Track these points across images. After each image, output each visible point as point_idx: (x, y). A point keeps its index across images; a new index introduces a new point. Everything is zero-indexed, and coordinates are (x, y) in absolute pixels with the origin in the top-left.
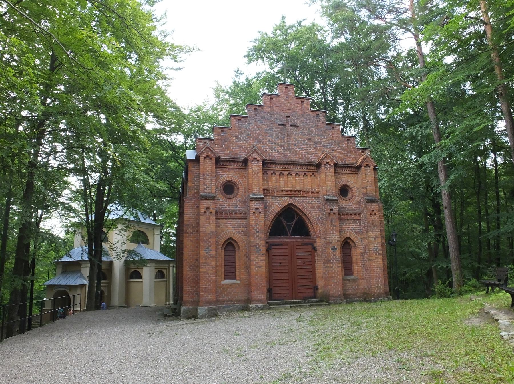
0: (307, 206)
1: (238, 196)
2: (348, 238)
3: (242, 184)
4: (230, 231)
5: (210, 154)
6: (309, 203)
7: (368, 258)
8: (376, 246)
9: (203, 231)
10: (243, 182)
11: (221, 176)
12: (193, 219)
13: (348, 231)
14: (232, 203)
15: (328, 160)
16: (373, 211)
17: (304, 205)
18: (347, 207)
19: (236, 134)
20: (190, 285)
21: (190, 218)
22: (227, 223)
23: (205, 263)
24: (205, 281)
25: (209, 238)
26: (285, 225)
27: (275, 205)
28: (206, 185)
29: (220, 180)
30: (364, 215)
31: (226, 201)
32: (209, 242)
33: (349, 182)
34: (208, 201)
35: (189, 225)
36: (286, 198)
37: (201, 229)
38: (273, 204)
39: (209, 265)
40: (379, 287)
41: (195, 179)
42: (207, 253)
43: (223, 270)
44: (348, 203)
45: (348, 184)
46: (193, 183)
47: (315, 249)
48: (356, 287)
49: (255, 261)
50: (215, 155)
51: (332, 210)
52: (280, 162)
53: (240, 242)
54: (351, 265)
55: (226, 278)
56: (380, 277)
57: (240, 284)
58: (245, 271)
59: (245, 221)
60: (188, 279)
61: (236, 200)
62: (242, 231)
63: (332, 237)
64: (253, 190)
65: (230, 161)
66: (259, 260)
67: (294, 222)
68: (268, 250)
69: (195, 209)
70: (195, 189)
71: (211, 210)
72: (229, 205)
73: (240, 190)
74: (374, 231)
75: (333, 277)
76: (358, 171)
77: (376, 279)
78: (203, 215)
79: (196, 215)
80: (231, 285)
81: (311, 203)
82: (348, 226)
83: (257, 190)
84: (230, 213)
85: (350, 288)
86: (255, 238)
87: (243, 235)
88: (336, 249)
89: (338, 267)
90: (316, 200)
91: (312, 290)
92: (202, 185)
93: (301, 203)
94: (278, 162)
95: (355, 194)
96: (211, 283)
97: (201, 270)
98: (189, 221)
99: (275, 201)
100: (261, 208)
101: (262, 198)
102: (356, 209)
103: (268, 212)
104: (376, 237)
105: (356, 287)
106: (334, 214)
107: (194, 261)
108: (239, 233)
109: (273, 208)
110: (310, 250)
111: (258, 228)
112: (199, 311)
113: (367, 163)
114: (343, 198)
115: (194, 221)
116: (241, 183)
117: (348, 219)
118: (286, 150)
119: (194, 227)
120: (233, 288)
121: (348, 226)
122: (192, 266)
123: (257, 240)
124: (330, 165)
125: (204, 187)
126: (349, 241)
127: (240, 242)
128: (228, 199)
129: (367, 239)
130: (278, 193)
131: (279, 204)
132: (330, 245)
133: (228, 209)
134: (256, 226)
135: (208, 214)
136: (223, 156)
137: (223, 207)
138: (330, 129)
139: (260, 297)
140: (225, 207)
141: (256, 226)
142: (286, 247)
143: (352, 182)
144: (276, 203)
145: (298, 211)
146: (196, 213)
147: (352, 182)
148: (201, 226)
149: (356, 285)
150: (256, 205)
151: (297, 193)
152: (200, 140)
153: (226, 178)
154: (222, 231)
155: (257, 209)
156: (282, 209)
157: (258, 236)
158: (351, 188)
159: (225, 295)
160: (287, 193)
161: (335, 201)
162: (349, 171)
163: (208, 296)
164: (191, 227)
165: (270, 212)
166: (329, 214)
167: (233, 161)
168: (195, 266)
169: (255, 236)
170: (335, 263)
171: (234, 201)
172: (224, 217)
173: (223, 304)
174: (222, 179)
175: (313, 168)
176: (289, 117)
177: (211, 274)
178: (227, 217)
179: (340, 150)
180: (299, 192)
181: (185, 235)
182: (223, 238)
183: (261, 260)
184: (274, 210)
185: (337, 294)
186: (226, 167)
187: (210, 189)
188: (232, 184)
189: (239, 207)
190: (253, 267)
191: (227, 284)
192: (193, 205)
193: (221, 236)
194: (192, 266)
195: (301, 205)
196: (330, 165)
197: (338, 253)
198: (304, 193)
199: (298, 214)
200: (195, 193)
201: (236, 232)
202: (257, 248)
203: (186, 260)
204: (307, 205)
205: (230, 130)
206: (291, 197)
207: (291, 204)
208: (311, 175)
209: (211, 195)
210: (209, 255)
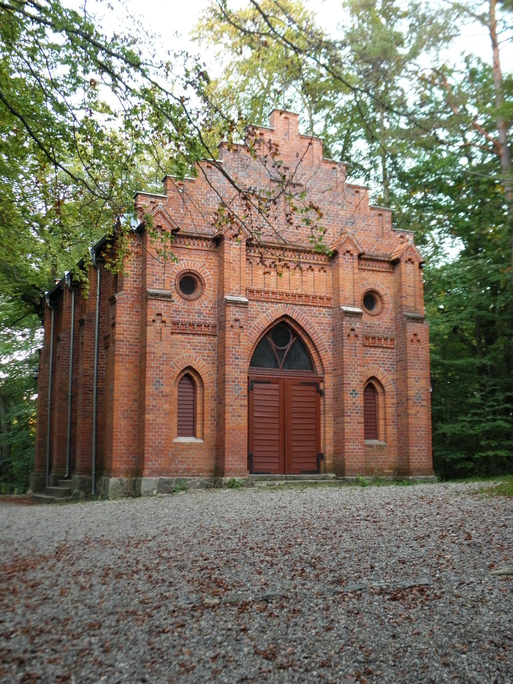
0: (312, 320)
1: (203, 298)
2: (373, 378)
3: (210, 277)
4: (190, 356)
5: (162, 223)
6: (315, 317)
7: (404, 412)
8: (418, 393)
9: (150, 353)
10: (211, 275)
11: (177, 262)
12: (130, 331)
13: (373, 367)
14: (193, 309)
15: (350, 248)
16: (415, 335)
17: (306, 319)
18: (373, 327)
19: (202, 192)
20: (123, 442)
21: (124, 330)
22: (184, 342)
23: (153, 406)
24: (153, 436)
25: (160, 364)
26: (274, 350)
27: (262, 316)
28: (155, 276)
29: (176, 269)
30: (401, 342)
31: (184, 305)
32: (160, 371)
33: (378, 285)
34: (160, 303)
35: (122, 341)
36: (280, 305)
37: (148, 349)
38: (258, 315)
39: (158, 410)
40: (421, 459)
41: (133, 264)
42: (156, 389)
43: (176, 420)
44: (375, 321)
45: (377, 289)
46: (131, 271)
47: (321, 393)
48: (382, 458)
49: (232, 406)
50: (172, 226)
51: (353, 330)
52: (272, 245)
53: (205, 374)
54: (376, 422)
55: (180, 435)
56: (422, 443)
57: (203, 444)
58: (211, 424)
59: (213, 340)
60: (120, 432)
61: (201, 304)
62: (208, 356)
63: (351, 375)
64: (230, 289)
65: (192, 238)
66: (237, 406)
67: (288, 346)
68: (250, 389)
69: (134, 315)
70: (135, 281)
71: (164, 318)
72: (188, 312)
73: (207, 287)
74: (417, 369)
75: (351, 439)
76: (393, 269)
77: (416, 446)
78: (152, 326)
79: (135, 325)
80: (190, 446)
81: (318, 317)
82: (374, 357)
83: (236, 290)
84: (190, 325)
85: (372, 459)
86: (233, 368)
87: (209, 363)
88: (356, 394)
89: (359, 423)
90: (326, 311)
91: (314, 460)
92: (150, 274)
93: (302, 315)
94: (270, 245)
95: (386, 306)
96: (162, 439)
97: (147, 416)
98: (123, 334)
99: (261, 309)
100: (243, 319)
101: (246, 304)
102: (388, 331)
103: (250, 327)
104: (419, 378)
105: (382, 458)
106: (356, 336)
107: (131, 403)
108: (204, 360)
109: (258, 321)
110: (313, 394)
111: (238, 352)
112: (143, 483)
113: (410, 257)
114: (367, 311)
115: (132, 335)
116: (208, 276)
117: (375, 347)
118: (281, 225)
119: (132, 345)
120: (192, 450)
121: (374, 357)
122: (127, 411)
123: (236, 372)
124: (351, 255)
125: (153, 279)
126: (373, 382)
127: (205, 374)
128: (186, 302)
129: (404, 382)
130: (274, 297)
131: (267, 315)
132: (347, 387)
133: (187, 319)
134: (235, 348)
135: (158, 324)
136: (184, 230)
137: (179, 315)
138: (353, 195)
139: (238, 465)
140: (182, 315)
141: (235, 348)
142: (277, 386)
143: (383, 286)
144: (263, 312)
145: (296, 328)
146: (135, 321)
147: (383, 286)
148: (148, 344)
149: (384, 455)
150: (235, 315)
151: (297, 298)
152: (145, 198)
153: (185, 266)
154: (177, 354)
155: (236, 320)
156: (272, 323)
157: (238, 365)
158: (380, 297)
159: (179, 461)
160: (281, 297)
161: (358, 315)
162: (379, 267)
163: (156, 461)
164: (125, 345)
165: (253, 328)
166: (349, 336)
167: (197, 238)
168: (132, 411)
169: (232, 365)
170: (355, 416)
171: (196, 305)
172: (305, 303)
173: (176, 476)
174: (178, 266)
175: (323, 258)
176: (288, 168)
177: (162, 425)
178: (185, 332)
179: (367, 230)
180: (300, 296)
181: (116, 358)
182: (177, 366)
183: (241, 406)
184: (259, 325)
185: (355, 467)
186: (185, 246)
187: (161, 283)
188: (193, 276)
189: (204, 316)
190: (228, 416)
191: (182, 444)
192: (130, 307)
193: (174, 363)
194: (127, 411)
195: (303, 318)
196: (351, 255)
197: (360, 400)
198: (307, 299)
199: (295, 334)
200: (134, 288)
201: (198, 358)
202: (235, 385)
203: (118, 400)
204: (311, 319)
205: (193, 184)
206: (287, 304)
207: (286, 316)
208: (320, 270)
209: (163, 292)
210: (159, 392)
